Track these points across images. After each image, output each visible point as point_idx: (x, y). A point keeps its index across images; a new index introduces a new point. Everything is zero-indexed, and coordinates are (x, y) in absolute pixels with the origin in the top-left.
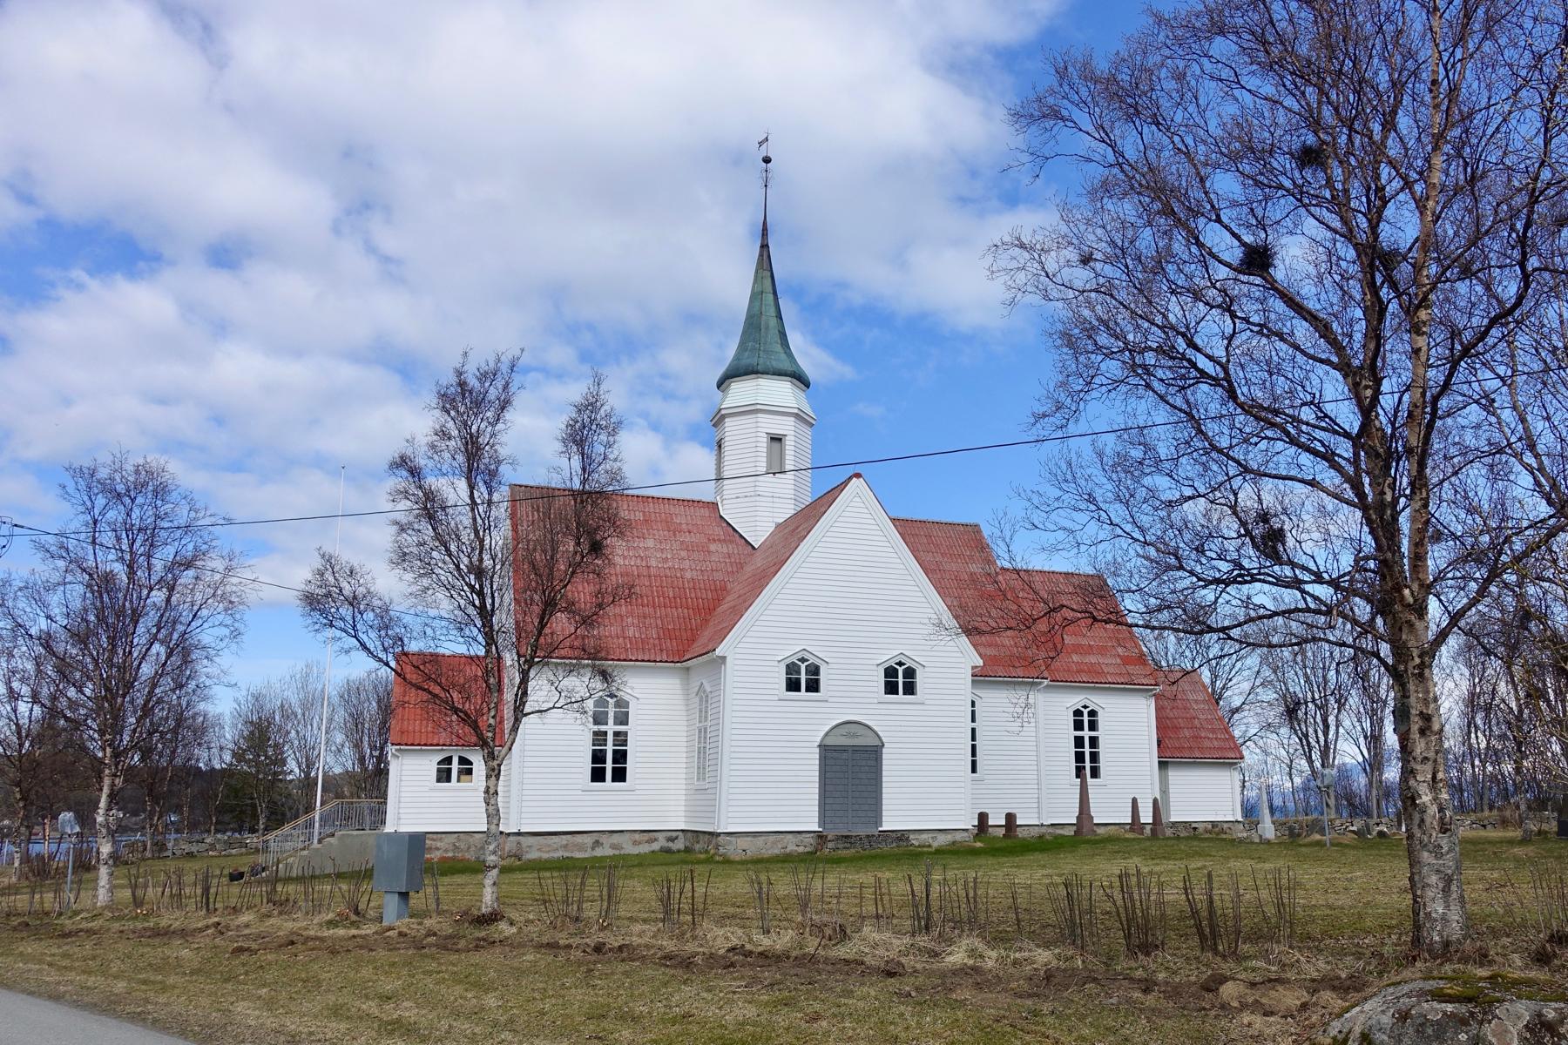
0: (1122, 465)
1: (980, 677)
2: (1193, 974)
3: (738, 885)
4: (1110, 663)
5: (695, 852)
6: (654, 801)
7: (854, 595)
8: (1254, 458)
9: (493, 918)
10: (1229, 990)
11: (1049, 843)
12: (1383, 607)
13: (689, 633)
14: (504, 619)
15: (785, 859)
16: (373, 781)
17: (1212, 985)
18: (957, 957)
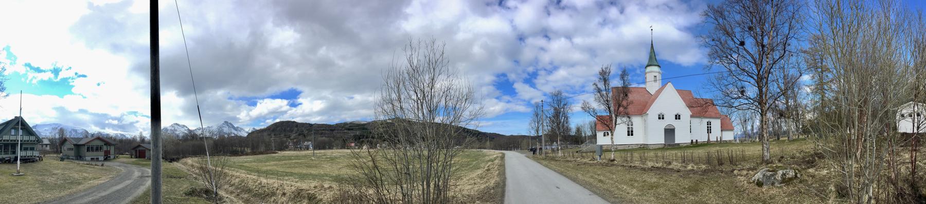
0: (718, 79)
1: (691, 116)
2: (729, 169)
3: (652, 154)
4: (713, 114)
5: (644, 148)
6: (638, 139)
7: (669, 102)
8: (741, 78)
9: (614, 160)
10: (735, 172)
11: (703, 145)
12: (760, 104)
13: (642, 111)
14: (612, 109)
15: (659, 149)
16: (595, 136)
17: (732, 171)
18: (690, 167)
